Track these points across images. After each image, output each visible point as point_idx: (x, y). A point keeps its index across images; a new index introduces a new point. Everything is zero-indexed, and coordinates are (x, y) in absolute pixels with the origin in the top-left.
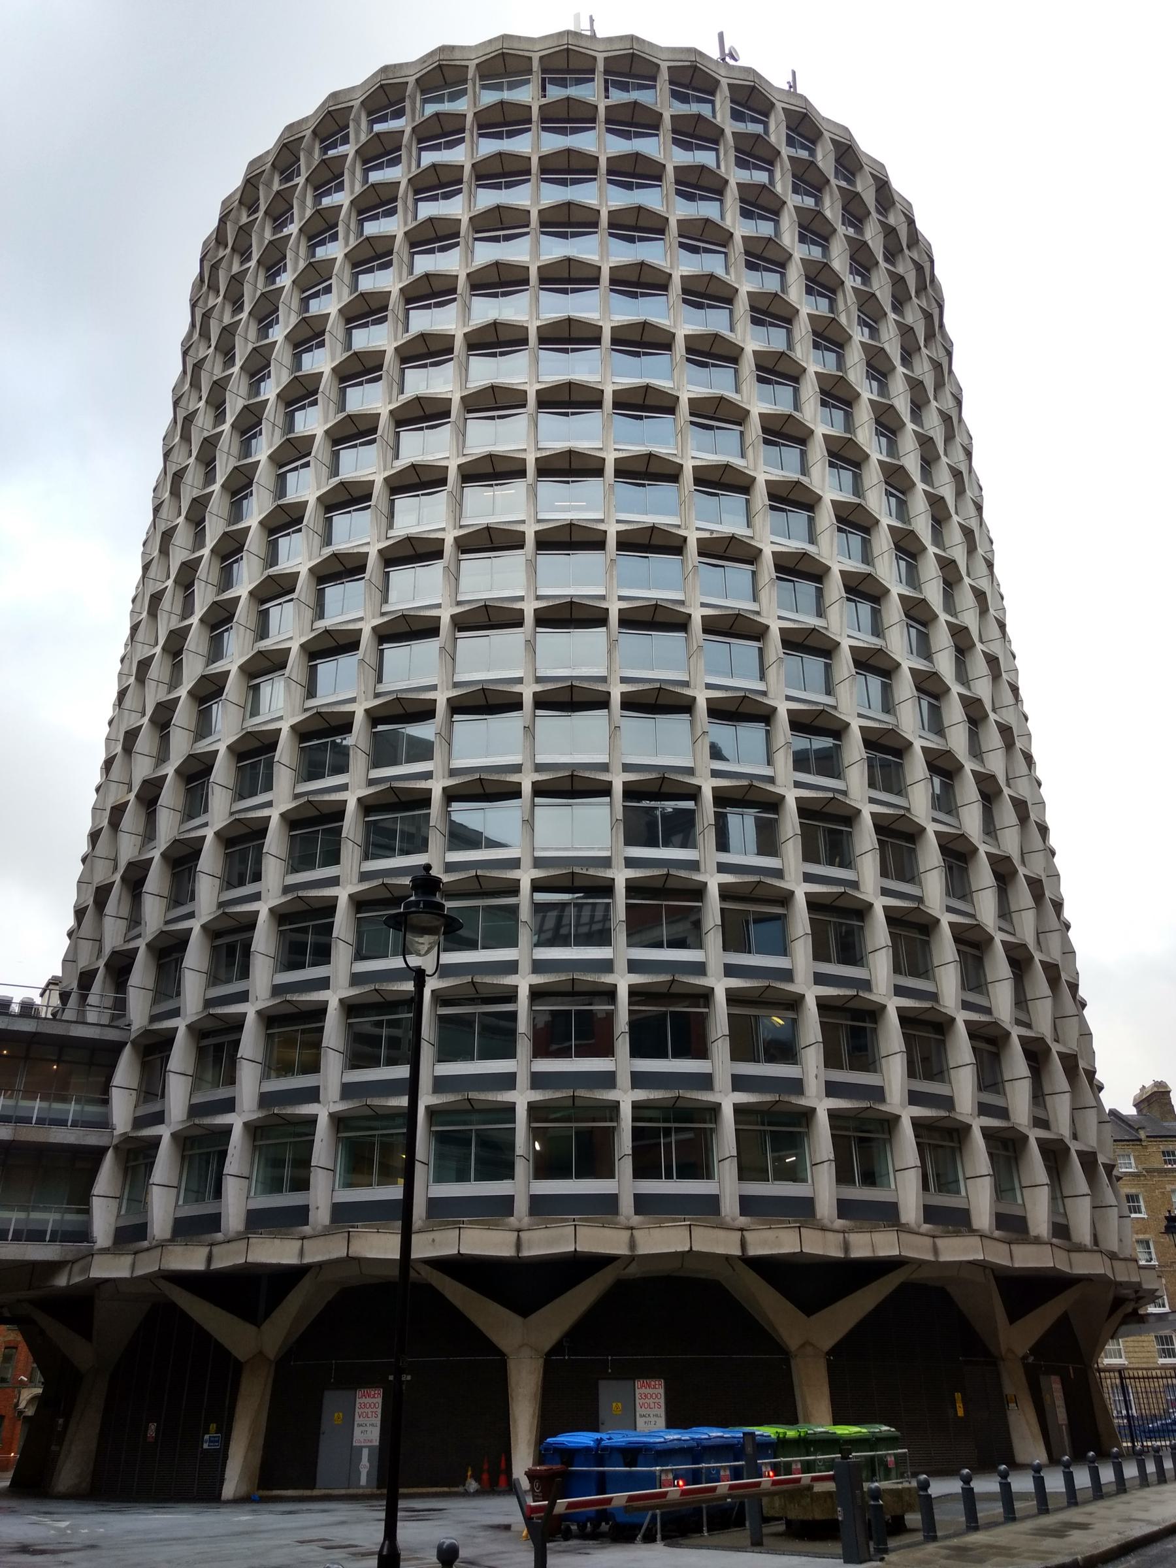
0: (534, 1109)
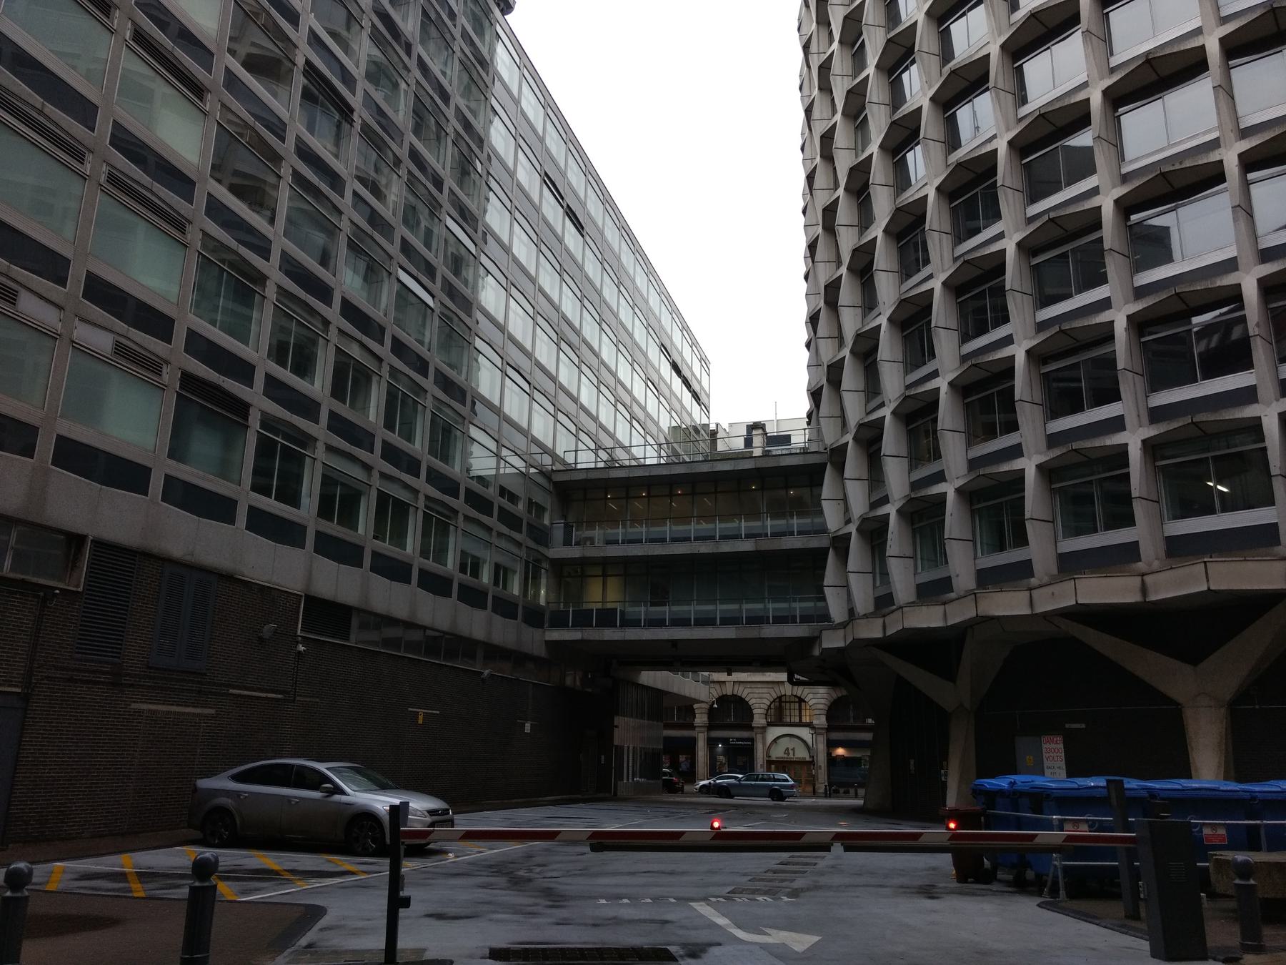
0: (1150, 447)
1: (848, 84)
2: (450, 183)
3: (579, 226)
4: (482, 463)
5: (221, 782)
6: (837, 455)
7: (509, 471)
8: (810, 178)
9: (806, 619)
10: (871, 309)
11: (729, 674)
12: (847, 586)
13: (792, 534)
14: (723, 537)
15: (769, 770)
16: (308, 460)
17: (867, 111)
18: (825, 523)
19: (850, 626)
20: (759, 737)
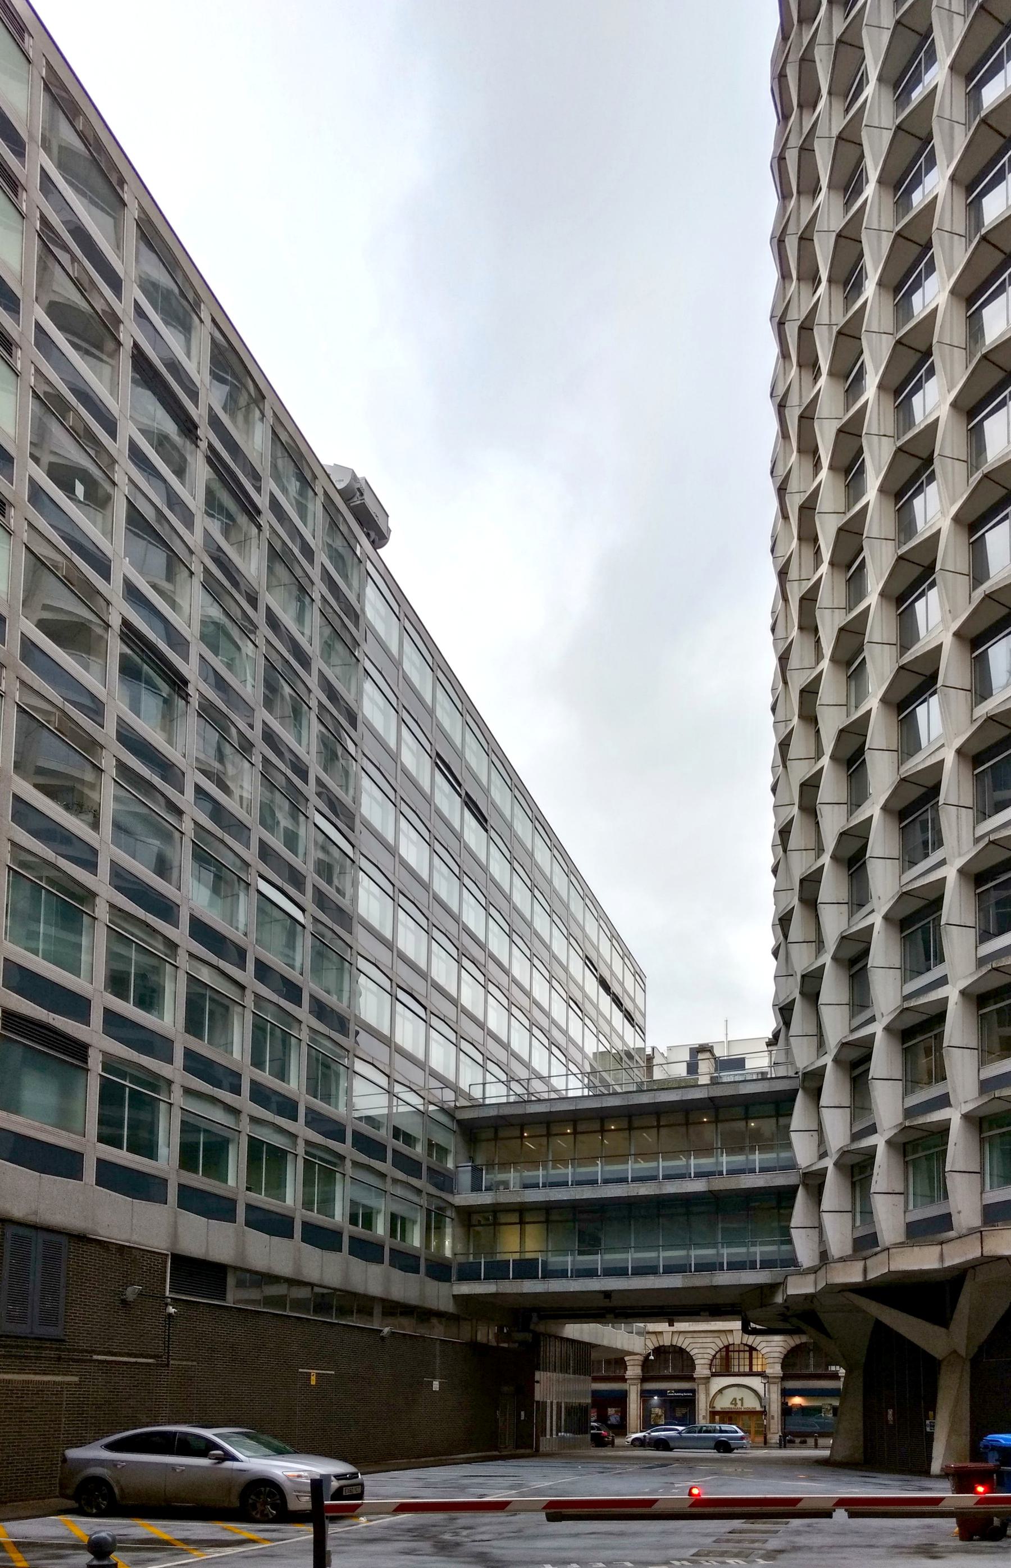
1: (841, 619)
2: (315, 770)
3: (482, 819)
4: (366, 1097)
5: (95, 1452)
6: (812, 1082)
7: (401, 1109)
8: (784, 746)
9: (767, 1264)
10: (861, 906)
11: (671, 1325)
12: (820, 1228)
13: (752, 1171)
14: (667, 1177)
15: (712, 1421)
16: (163, 1106)
17: (865, 653)
18: (793, 1159)
19: (823, 1270)
20: (702, 1388)
